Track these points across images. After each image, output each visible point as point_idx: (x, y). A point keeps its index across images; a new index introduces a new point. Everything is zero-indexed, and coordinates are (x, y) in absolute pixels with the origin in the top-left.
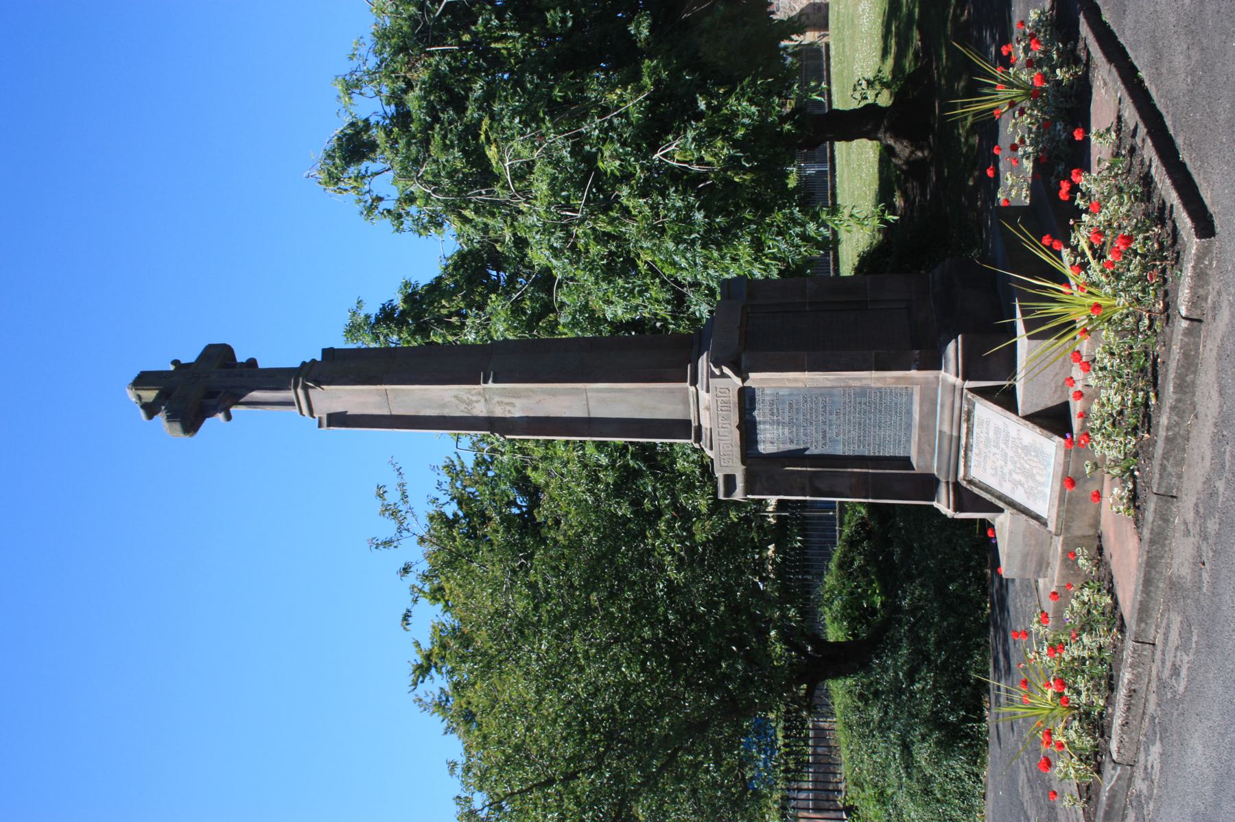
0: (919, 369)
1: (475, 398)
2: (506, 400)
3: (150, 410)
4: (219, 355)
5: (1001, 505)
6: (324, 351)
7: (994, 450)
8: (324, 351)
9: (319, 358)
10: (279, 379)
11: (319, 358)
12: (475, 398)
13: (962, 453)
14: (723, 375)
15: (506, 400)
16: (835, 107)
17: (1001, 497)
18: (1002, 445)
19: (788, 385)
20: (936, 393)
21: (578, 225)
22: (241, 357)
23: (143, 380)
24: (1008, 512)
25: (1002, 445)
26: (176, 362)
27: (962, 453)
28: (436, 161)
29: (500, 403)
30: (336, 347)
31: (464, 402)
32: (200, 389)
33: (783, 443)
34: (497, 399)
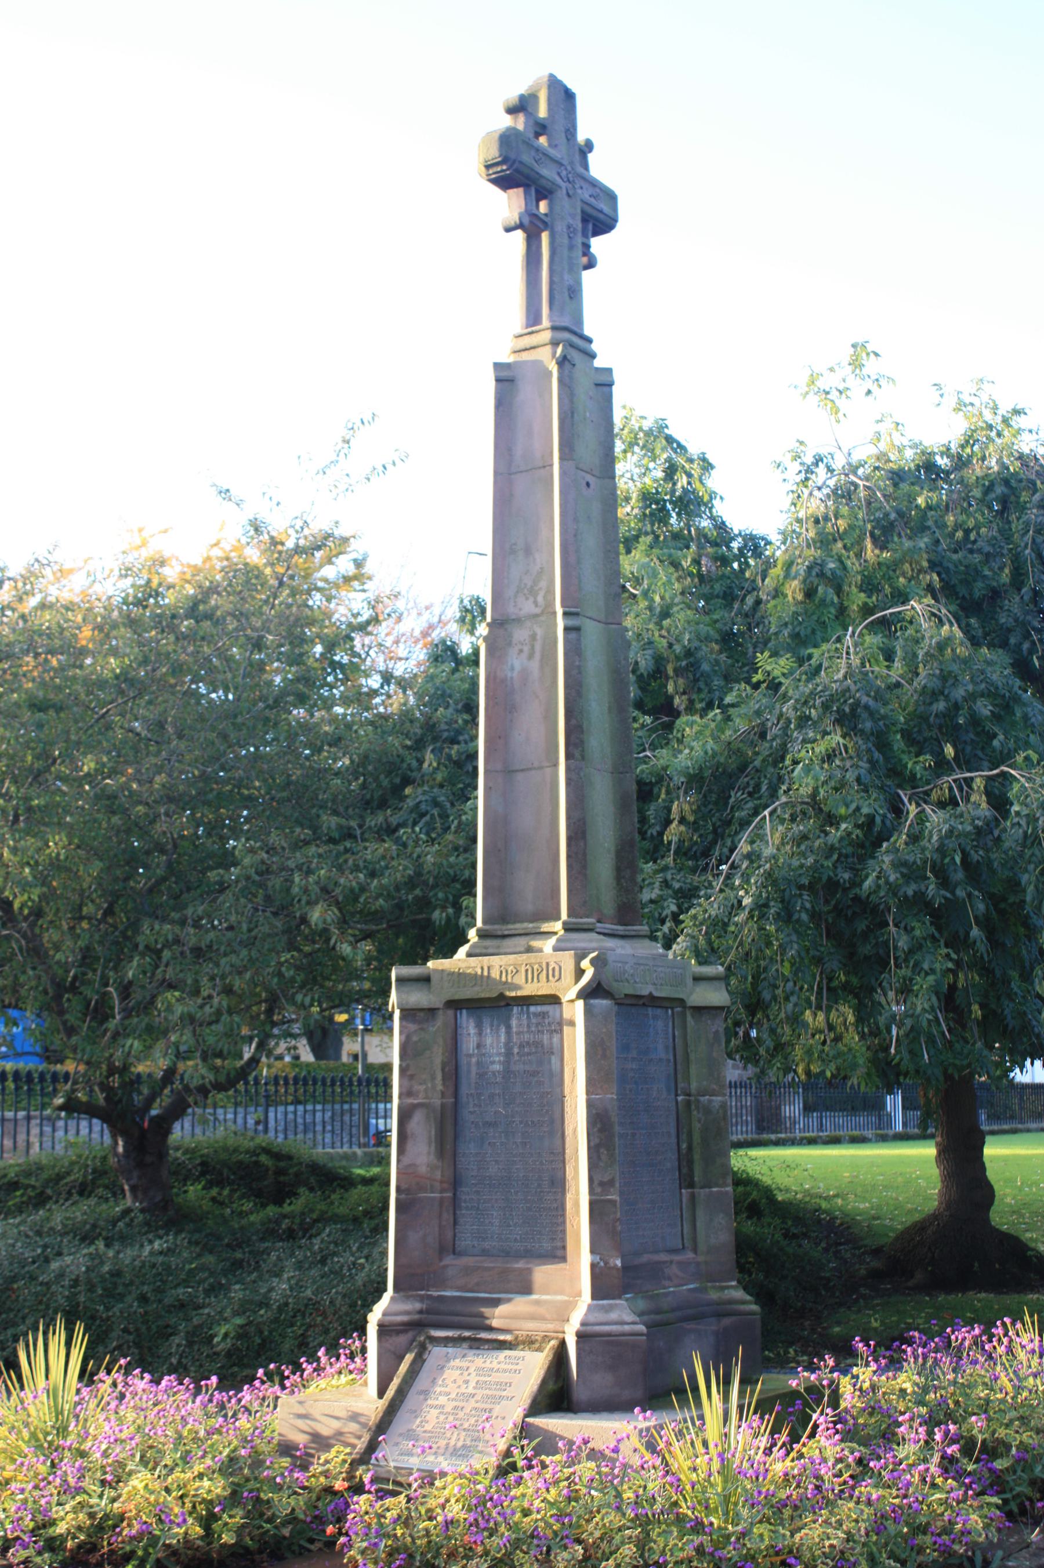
0: (593, 1266)
1: (540, 599)
2: (538, 647)
3: (521, 106)
4: (599, 218)
5: (390, 1393)
6: (609, 371)
7: (473, 1379)
8: (609, 371)
9: (598, 363)
10: (567, 296)
11: (598, 363)
12: (540, 599)
13: (467, 1334)
14: (580, 973)
15: (538, 647)
16: (988, 1139)
17: (402, 1393)
18: (480, 1393)
19: (566, 1070)
20: (556, 1293)
21: (77, 877)
22: (598, 244)
23: (564, 98)
24: (382, 1404)
25: (480, 1393)
26: (589, 146)
27: (467, 1334)
28: (225, 955)
29: (533, 637)
30: (615, 389)
31: (535, 582)
32: (549, 181)
33: (478, 1063)
34: (539, 632)
